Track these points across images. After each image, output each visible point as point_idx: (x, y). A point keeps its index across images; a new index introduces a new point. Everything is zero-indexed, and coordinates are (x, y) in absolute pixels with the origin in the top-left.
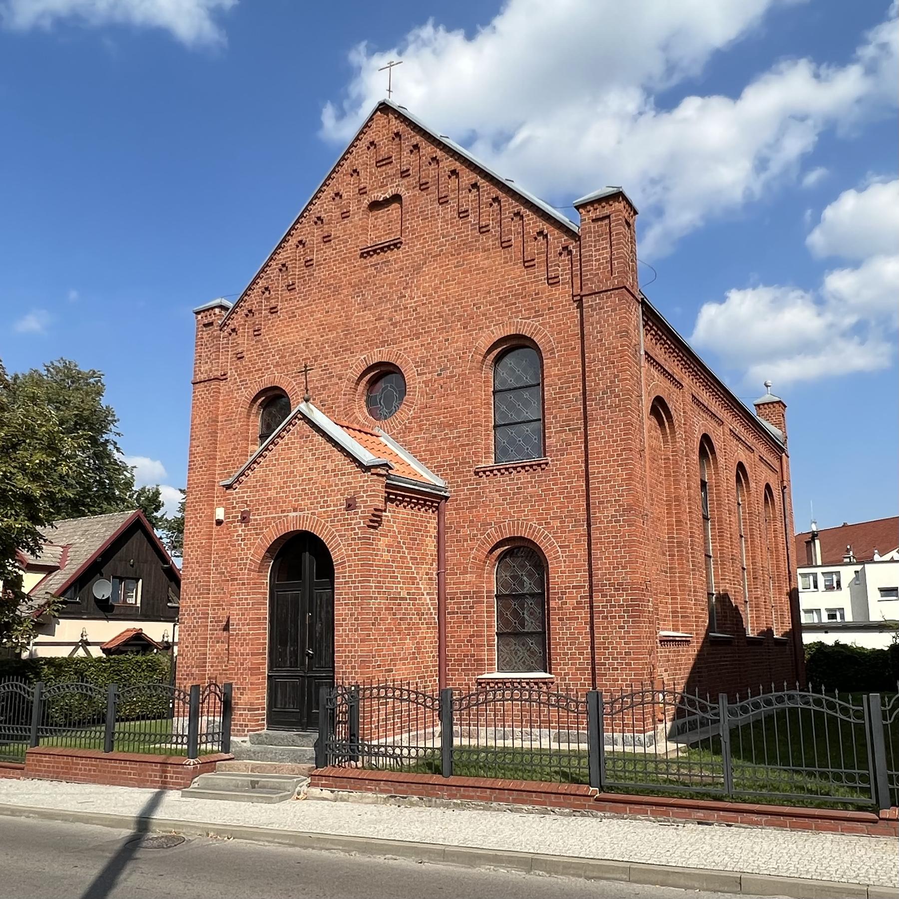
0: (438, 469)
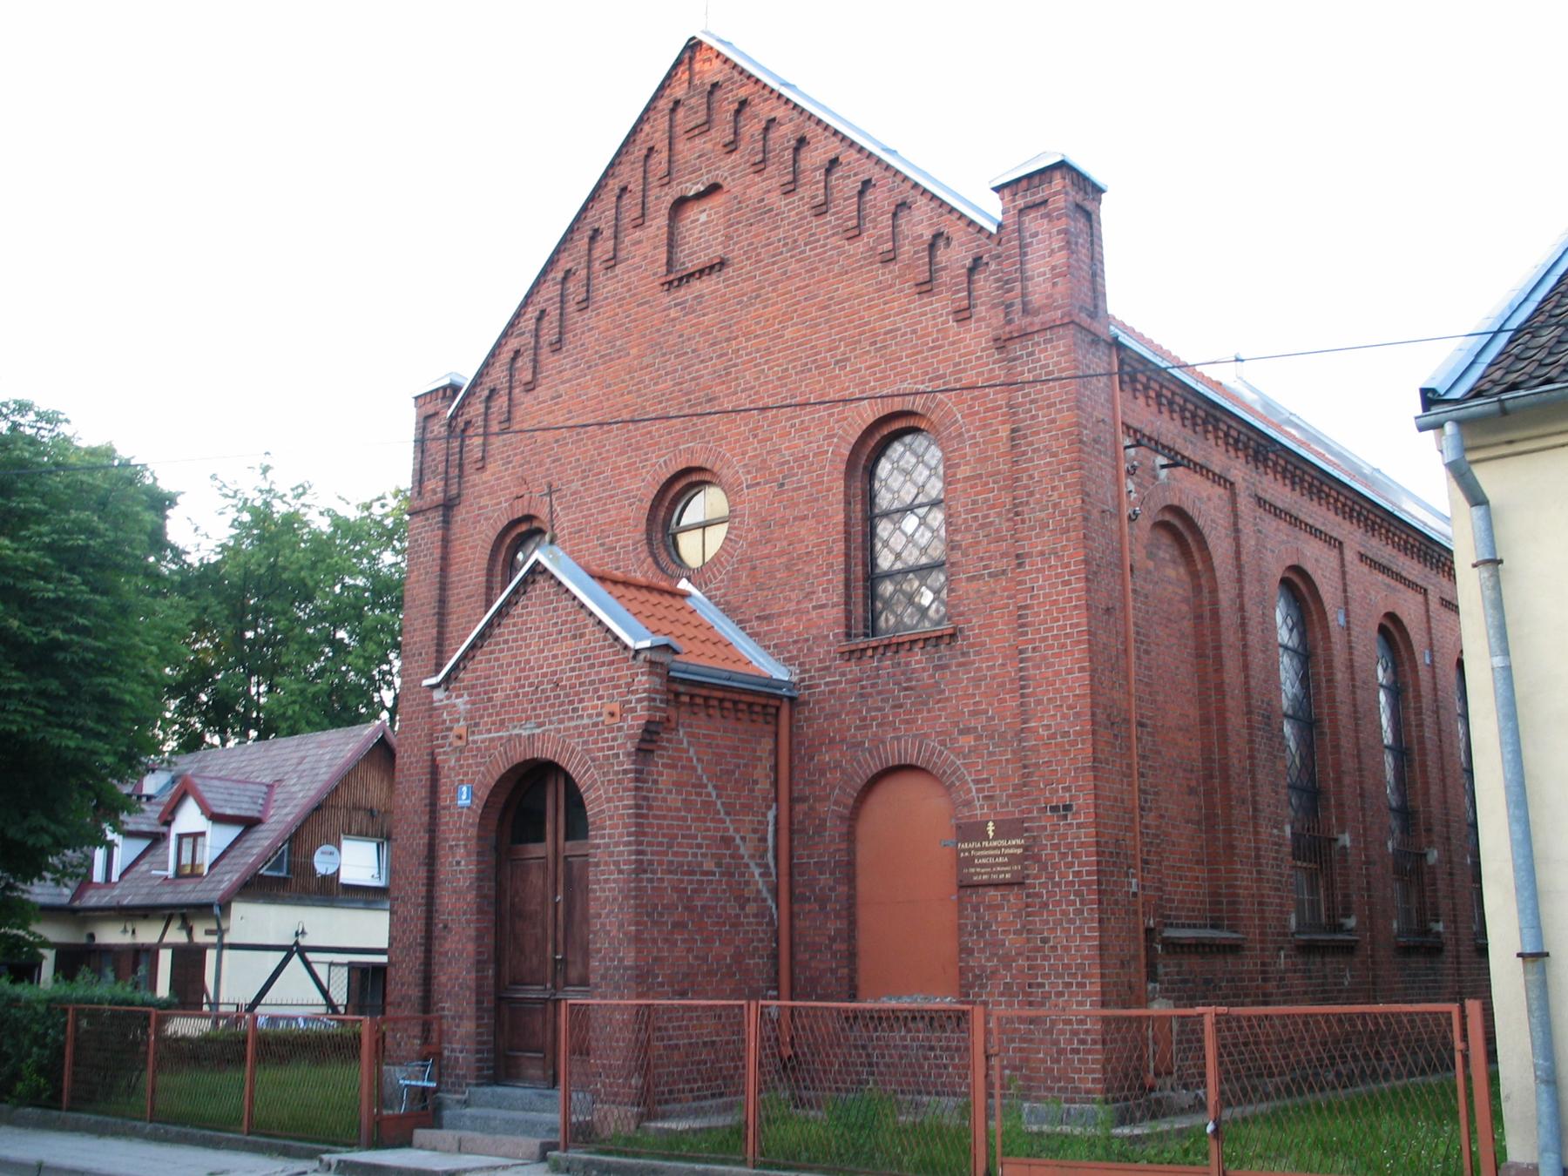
0: (777, 651)
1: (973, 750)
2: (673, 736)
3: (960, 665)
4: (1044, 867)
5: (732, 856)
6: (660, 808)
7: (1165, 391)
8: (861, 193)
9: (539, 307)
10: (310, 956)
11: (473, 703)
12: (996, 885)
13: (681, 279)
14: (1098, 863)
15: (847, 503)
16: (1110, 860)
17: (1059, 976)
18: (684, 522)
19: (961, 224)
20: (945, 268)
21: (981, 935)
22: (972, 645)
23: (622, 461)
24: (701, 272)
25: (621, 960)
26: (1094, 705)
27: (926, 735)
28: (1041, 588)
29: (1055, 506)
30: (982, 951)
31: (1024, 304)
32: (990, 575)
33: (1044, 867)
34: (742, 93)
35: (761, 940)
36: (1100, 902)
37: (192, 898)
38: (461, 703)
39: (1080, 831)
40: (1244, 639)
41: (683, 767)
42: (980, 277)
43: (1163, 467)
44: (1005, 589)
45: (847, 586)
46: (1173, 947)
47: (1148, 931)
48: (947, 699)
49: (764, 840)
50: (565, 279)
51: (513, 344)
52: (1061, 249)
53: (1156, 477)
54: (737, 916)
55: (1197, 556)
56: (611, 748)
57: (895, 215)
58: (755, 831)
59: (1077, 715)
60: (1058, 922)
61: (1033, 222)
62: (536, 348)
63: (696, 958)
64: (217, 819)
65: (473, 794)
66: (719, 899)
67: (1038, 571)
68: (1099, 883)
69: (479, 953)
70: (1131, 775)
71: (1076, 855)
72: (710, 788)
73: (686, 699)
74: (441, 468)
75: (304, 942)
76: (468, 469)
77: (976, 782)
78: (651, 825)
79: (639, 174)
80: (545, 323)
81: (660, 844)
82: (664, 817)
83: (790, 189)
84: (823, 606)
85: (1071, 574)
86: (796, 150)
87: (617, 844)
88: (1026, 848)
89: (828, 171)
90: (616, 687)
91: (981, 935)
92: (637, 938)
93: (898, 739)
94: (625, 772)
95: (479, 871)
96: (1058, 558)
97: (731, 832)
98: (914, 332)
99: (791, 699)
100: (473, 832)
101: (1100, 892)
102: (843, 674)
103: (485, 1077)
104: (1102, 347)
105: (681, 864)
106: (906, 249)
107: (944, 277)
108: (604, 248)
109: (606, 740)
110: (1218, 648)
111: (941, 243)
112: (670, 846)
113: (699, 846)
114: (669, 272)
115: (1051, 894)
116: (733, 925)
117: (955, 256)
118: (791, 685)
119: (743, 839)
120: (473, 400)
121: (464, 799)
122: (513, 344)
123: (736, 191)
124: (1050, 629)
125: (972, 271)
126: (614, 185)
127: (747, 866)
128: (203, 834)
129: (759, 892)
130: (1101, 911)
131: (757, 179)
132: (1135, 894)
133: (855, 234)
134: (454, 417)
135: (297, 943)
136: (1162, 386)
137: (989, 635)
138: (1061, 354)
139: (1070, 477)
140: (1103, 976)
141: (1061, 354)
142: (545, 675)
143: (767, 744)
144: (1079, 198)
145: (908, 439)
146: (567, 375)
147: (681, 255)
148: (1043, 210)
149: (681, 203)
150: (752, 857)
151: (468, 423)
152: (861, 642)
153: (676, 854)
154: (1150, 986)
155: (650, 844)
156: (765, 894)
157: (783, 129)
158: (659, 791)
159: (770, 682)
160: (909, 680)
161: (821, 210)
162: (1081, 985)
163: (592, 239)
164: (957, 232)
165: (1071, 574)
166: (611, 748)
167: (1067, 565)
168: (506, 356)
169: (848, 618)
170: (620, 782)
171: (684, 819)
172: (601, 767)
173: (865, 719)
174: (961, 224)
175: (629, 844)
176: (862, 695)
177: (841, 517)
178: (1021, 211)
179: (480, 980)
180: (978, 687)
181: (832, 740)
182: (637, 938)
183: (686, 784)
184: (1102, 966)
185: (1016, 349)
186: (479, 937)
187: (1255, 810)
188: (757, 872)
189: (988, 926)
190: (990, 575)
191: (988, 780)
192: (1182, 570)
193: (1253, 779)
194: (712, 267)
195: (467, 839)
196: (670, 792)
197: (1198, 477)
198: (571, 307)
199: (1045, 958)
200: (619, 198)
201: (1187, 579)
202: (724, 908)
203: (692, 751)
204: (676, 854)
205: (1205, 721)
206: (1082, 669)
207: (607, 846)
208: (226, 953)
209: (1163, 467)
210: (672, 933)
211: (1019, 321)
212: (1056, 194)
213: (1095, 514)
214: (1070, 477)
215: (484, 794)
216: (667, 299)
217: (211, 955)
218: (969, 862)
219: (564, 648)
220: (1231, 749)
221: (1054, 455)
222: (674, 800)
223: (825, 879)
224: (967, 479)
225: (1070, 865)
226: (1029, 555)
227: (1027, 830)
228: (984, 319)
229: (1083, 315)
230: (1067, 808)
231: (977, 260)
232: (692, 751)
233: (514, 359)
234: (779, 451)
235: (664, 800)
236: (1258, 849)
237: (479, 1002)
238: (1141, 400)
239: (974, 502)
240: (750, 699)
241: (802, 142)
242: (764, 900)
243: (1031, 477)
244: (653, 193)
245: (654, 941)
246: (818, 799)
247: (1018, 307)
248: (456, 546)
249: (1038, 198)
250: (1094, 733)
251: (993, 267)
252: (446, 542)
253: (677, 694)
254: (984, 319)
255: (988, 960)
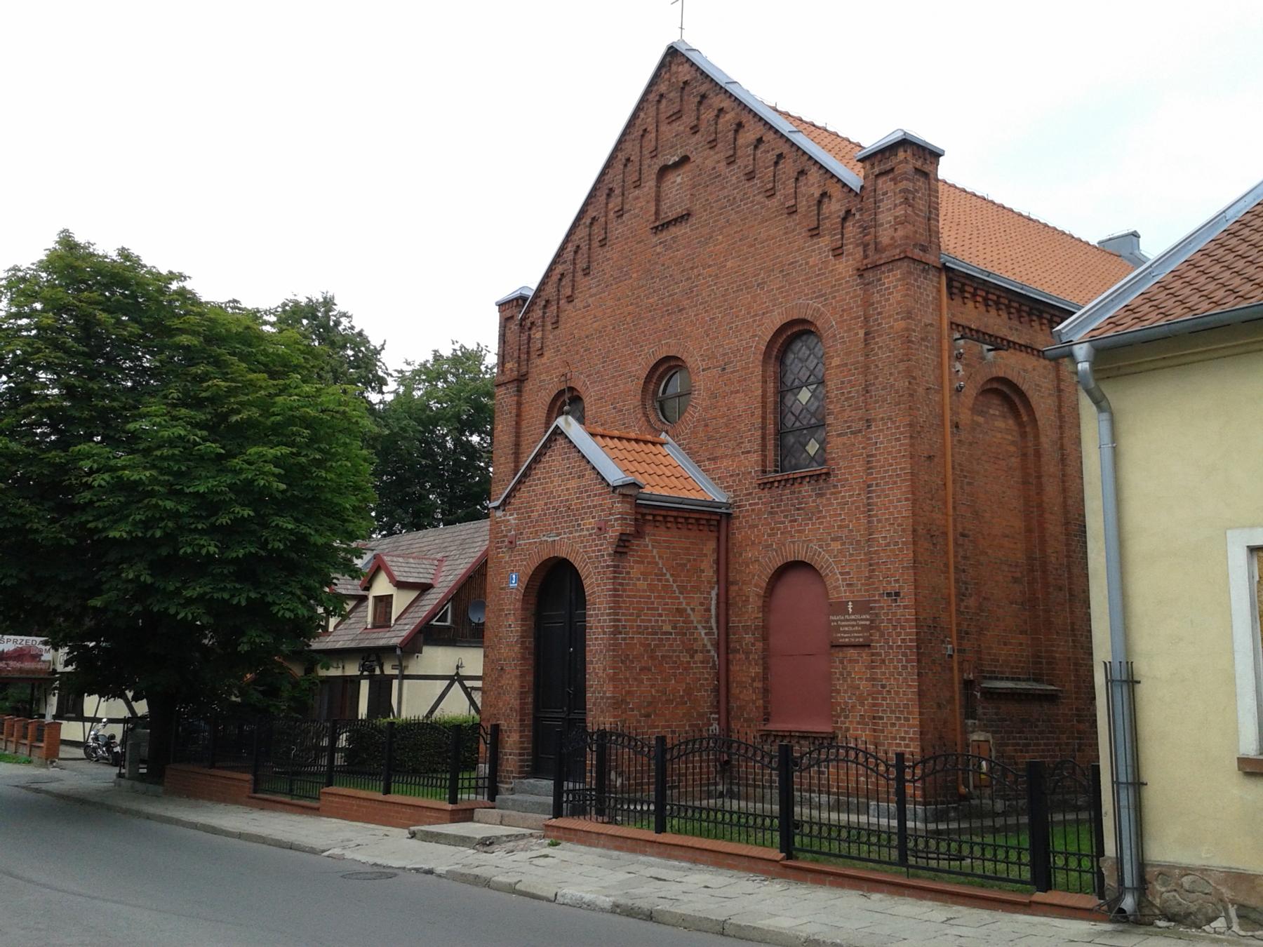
0: (718, 480)
1: (840, 551)
2: (641, 542)
3: (832, 494)
4: (882, 635)
5: (684, 622)
6: (631, 590)
7: (990, 296)
8: (776, 163)
9: (576, 243)
10: (468, 683)
11: (519, 519)
12: (854, 646)
13: (663, 225)
14: (917, 633)
15: (765, 382)
16: (927, 635)
17: (893, 712)
18: (670, 391)
19: (839, 185)
20: (827, 218)
21: (845, 680)
22: (839, 480)
23: (627, 351)
24: (676, 220)
25: (605, 693)
26: (915, 523)
27: (810, 541)
28: (882, 443)
29: (892, 386)
30: (846, 692)
31: (876, 243)
32: (852, 433)
33: (882, 635)
34: (703, 89)
35: (707, 679)
36: (919, 661)
37: (381, 643)
38: (512, 519)
39: (904, 611)
40: (1063, 470)
41: (649, 563)
42: (849, 224)
43: (989, 350)
44: (860, 443)
45: (763, 438)
46: (990, 694)
47: (968, 684)
48: (825, 517)
49: (708, 610)
50: (591, 224)
51: (559, 269)
52: (901, 203)
53: (983, 358)
54: (689, 663)
55: (1022, 411)
56: (599, 551)
57: (797, 179)
58: (702, 604)
59: (903, 530)
60: (892, 674)
61: (884, 184)
62: (574, 272)
63: (657, 691)
64: (401, 585)
65: (518, 580)
66: (674, 651)
67: (881, 431)
68: (918, 647)
69: (522, 687)
70: (947, 572)
71: (903, 628)
72: (668, 576)
73: (650, 518)
74: (516, 354)
75: (463, 672)
76: (534, 355)
77: (841, 574)
78: (624, 602)
79: (637, 149)
80: (579, 255)
81: (632, 614)
82: (635, 596)
83: (731, 161)
84: (748, 452)
85: (901, 433)
86: (736, 131)
87: (602, 615)
88: (872, 621)
89: (756, 147)
90: (603, 510)
91: (845, 680)
92: (613, 678)
93: (794, 543)
94: (608, 566)
95: (523, 631)
96: (894, 422)
97: (684, 606)
98: (807, 263)
99: (729, 515)
100: (518, 605)
101: (918, 654)
102: (760, 498)
103: (526, 772)
104: (932, 272)
105: (647, 628)
106: (803, 205)
107: (827, 224)
108: (615, 203)
109: (596, 545)
110: (1039, 477)
111: (826, 200)
112: (639, 615)
113: (660, 615)
114: (657, 219)
115: (887, 654)
116: (685, 669)
117: (835, 207)
118: (728, 506)
119: (693, 610)
120: (535, 307)
121: (514, 584)
122: (559, 269)
123: (699, 161)
124: (886, 471)
125: (844, 219)
126: (621, 156)
127: (696, 628)
128: (391, 596)
129: (704, 645)
130: (919, 668)
131: (712, 153)
132: (951, 656)
133: (771, 194)
134: (523, 319)
135: (457, 674)
136: (987, 293)
137: (851, 474)
138: (899, 280)
139: (902, 367)
140: (921, 714)
141: (899, 280)
142: (561, 501)
143: (712, 545)
144: (919, 164)
145: (804, 338)
146: (594, 291)
147: (664, 206)
148: (891, 176)
149: (664, 170)
150: (699, 622)
151: (532, 323)
152: (771, 476)
153: (642, 621)
154: (970, 722)
155: (623, 614)
156: (709, 647)
157: (728, 117)
158: (630, 579)
159: (712, 504)
160: (800, 503)
161: (750, 176)
162: (907, 719)
163: (609, 195)
164: (835, 191)
165: (901, 433)
166: (599, 551)
167: (898, 428)
168: (555, 278)
169: (764, 461)
170: (604, 573)
171: (649, 597)
172: (593, 563)
173: (772, 529)
174: (839, 185)
175: (609, 614)
176: (771, 513)
177: (760, 392)
178: (877, 176)
179: (523, 705)
180: (843, 509)
181: (753, 543)
182: (613, 678)
183: (650, 574)
184: (920, 707)
185: (870, 276)
186: (522, 675)
187: (1071, 595)
188: (703, 632)
189: (849, 674)
190: (852, 433)
191: (848, 573)
192: (1011, 422)
193: (1069, 572)
194: (683, 216)
195: (515, 610)
196: (639, 579)
197: (1024, 355)
198: (595, 244)
199: (884, 699)
200: (625, 165)
201: (1016, 428)
202: (678, 657)
203: (655, 551)
204: (642, 621)
205: (1029, 530)
206: (907, 499)
207: (597, 615)
208: (405, 682)
209: (989, 350)
210: (639, 674)
211: (873, 257)
212: (901, 162)
213: (921, 390)
214: (902, 367)
215: (525, 580)
216: (655, 239)
217: (395, 683)
218: (837, 629)
219: (572, 484)
220: (1049, 551)
221: (892, 351)
222: (642, 585)
223: (748, 637)
224: (838, 366)
225: (899, 634)
226: (874, 420)
227: (871, 608)
228: (851, 254)
229: (917, 251)
230: (897, 594)
231: (848, 212)
232: (655, 551)
233: (560, 280)
234: (722, 346)
235: (635, 585)
236: (1073, 624)
237: (521, 720)
238: (970, 304)
239: (843, 383)
240: (697, 516)
241: (740, 125)
242: (709, 651)
243: (877, 366)
244: (647, 162)
245: (627, 680)
246: (744, 583)
247: (872, 246)
248: (525, 408)
249: (888, 167)
250: (915, 543)
251: (858, 216)
252: (519, 404)
253: (644, 515)
254: (851, 254)
255: (850, 698)
